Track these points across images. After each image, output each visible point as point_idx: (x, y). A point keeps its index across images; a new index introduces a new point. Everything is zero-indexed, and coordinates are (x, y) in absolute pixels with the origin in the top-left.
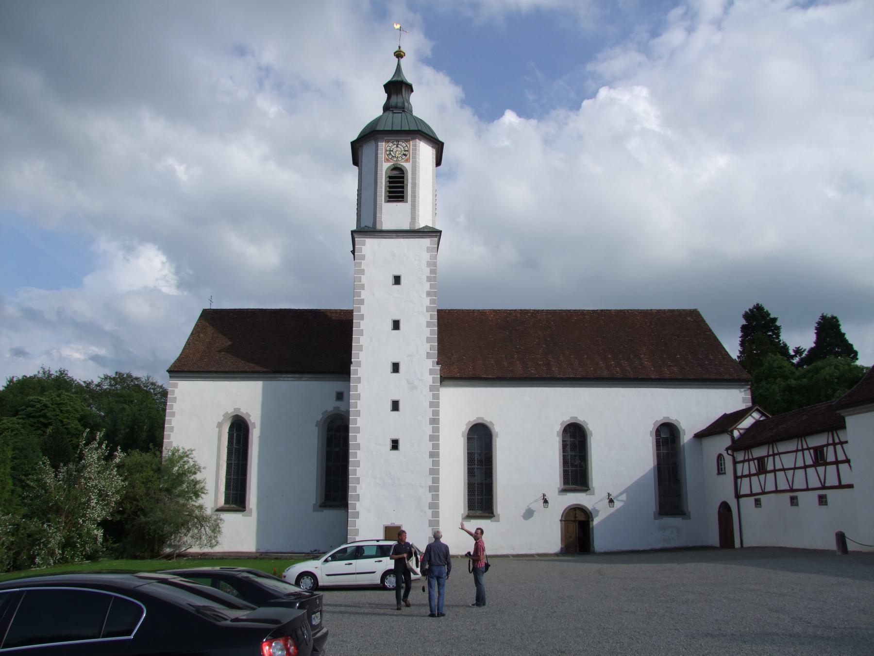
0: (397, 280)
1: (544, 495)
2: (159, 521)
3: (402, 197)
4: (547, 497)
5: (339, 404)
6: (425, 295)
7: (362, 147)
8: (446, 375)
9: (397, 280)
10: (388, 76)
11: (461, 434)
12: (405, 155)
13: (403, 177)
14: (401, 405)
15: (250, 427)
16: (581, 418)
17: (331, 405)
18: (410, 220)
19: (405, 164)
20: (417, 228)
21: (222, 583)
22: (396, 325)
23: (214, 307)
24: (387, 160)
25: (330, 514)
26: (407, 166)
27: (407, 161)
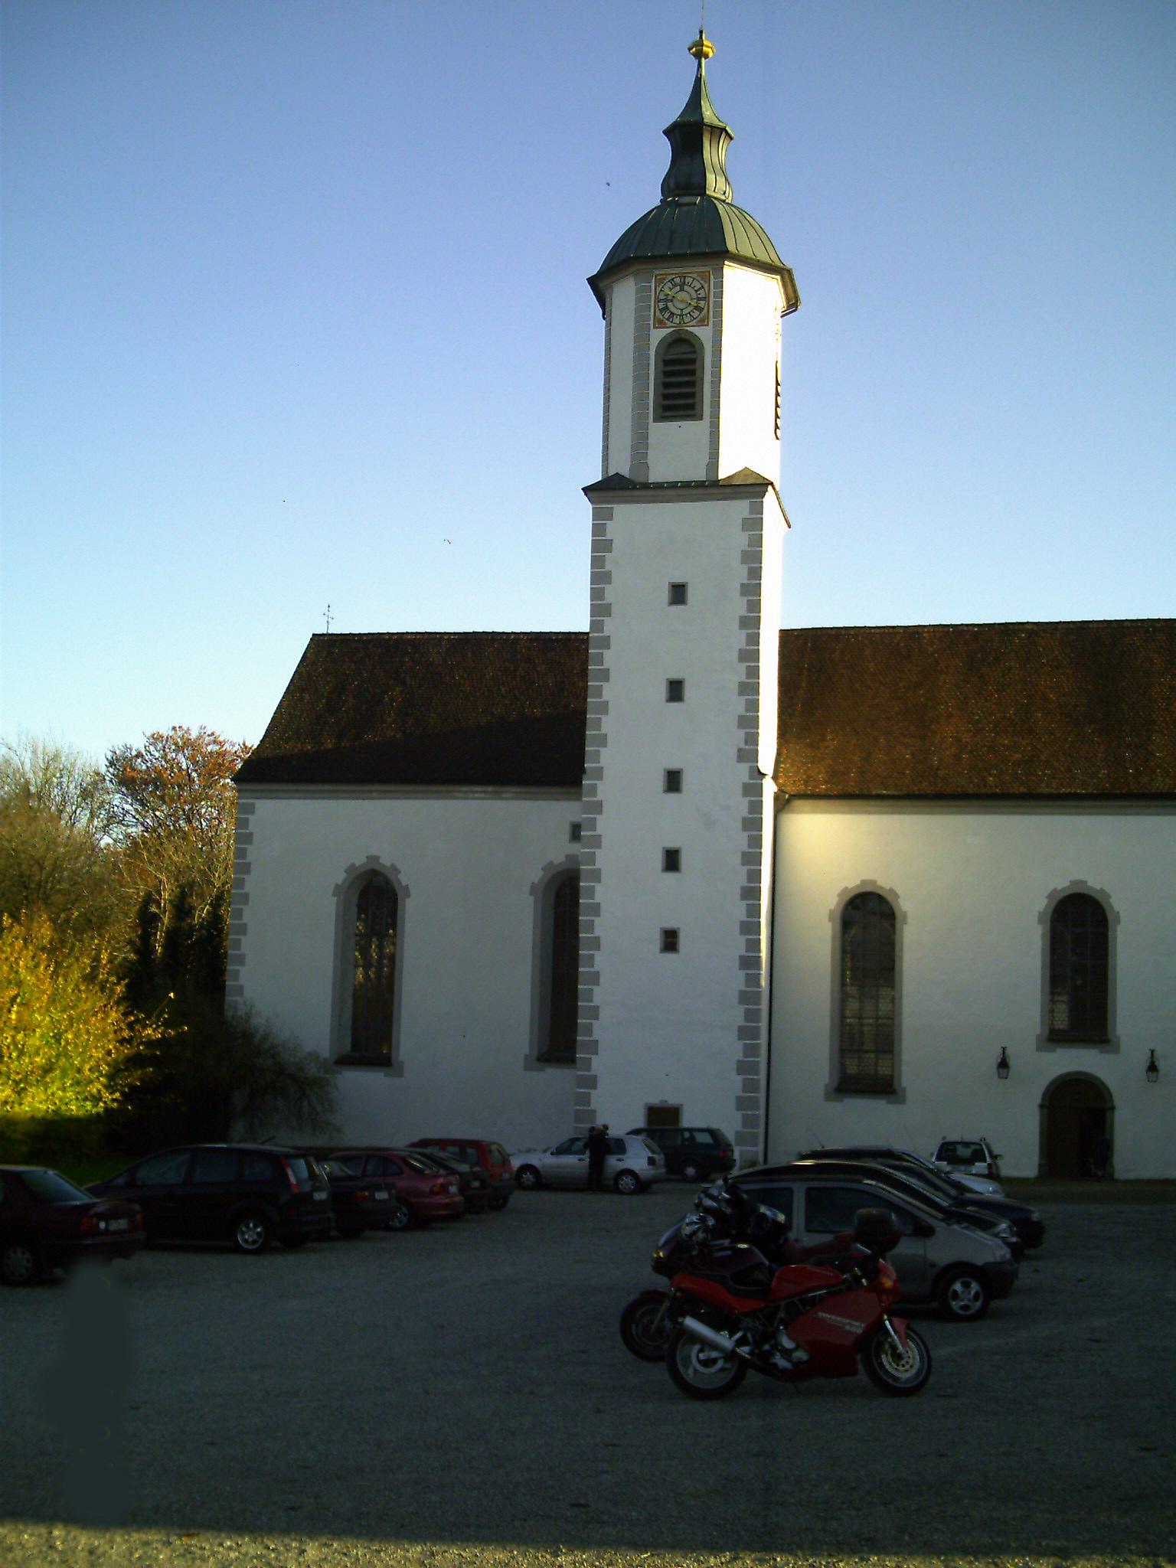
0: (678, 594)
1: (1152, 1052)
2: (799, 1373)
3: (692, 407)
4: (1161, 1064)
5: (576, 849)
6: (736, 624)
7: (611, 287)
8: (791, 789)
9: (678, 594)
10: (673, 112)
11: (1107, 888)
12: (700, 310)
13: (693, 361)
14: (685, 860)
15: (400, 895)
16: (1095, 882)
17: (559, 850)
18: (707, 460)
19: (698, 331)
20: (723, 473)
21: (291, 1151)
22: (676, 690)
23: (335, 629)
24: (660, 324)
25: (556, 1076)
26: (703, 333)
27: (703, 322)
